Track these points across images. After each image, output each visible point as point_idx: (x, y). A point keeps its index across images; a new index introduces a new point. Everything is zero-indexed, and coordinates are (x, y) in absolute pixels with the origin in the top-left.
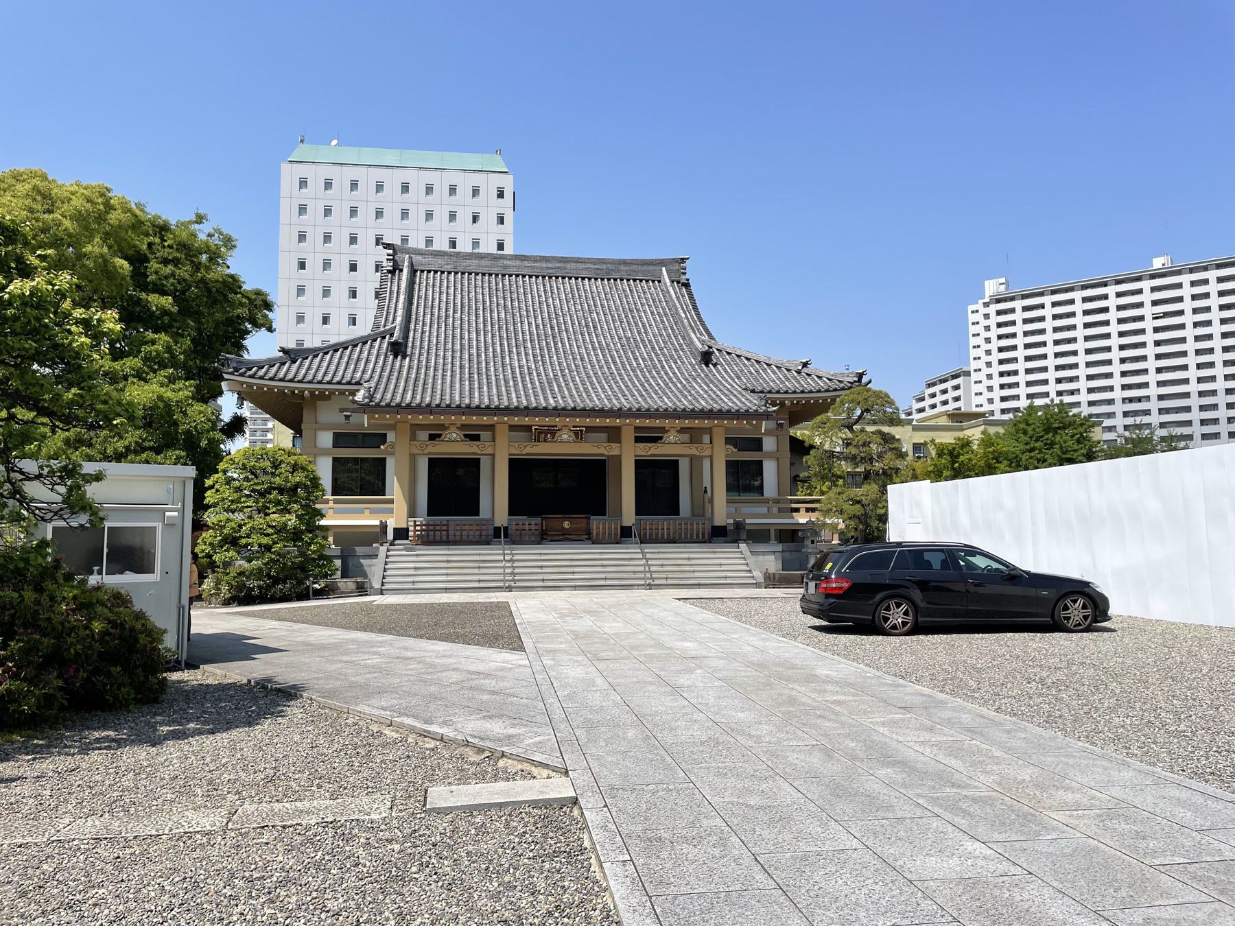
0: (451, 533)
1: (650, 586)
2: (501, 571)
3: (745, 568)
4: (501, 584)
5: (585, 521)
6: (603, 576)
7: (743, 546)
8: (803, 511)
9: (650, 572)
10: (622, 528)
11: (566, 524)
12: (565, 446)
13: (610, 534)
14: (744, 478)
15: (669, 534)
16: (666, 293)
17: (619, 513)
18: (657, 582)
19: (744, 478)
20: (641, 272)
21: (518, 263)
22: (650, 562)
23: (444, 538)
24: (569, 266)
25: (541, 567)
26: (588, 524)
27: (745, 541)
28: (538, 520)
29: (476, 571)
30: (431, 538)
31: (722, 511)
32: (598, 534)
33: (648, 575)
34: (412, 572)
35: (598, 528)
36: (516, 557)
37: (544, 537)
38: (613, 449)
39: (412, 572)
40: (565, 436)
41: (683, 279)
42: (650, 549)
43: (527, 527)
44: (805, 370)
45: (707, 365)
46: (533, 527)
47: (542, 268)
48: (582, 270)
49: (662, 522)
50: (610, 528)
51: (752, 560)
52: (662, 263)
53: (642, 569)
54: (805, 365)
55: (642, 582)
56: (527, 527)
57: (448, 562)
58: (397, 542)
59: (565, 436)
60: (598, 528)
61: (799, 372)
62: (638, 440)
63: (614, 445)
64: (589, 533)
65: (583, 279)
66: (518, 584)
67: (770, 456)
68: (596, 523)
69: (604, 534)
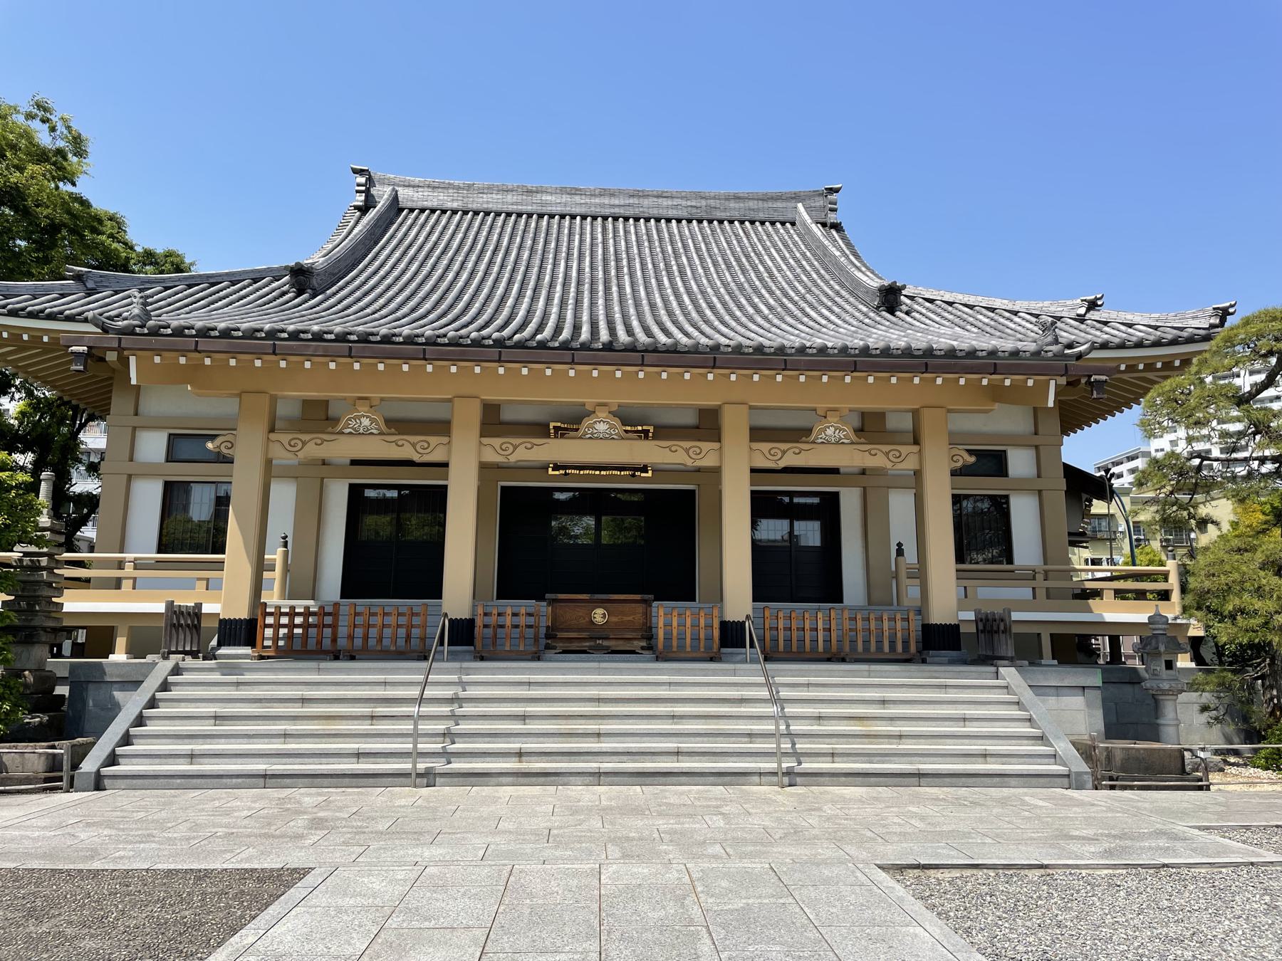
0: (343, 631)
1: (791, 778)
2: (407, 727)
3: (1026, 730)
4: (406, 766)
5: (640, 608)
6: (671, 745)
7: (1009, 673)
8: (1108, 596)
9: (786, 718)
10: (724, 625)
11: (599, 615)
12: (601, 449)
13: (696, 639)
14: (983, 533)
15: (828, 641)
16: (806, 235)
17: (718, 596)
18: (808, 765)
19: (983, 533)
20: (768, 214)
21: (565, 198)
22: (790, 710)
23: (327, 643)
24: (646, 202)
25: (524, 718)
26: (647, 615)
27: (1012, 661)
28: (543, 608)
29: (365, 727)
30: (312, 644)
31: (947, 597)
32: (668, 638)
33: (786, 746)
34: (208, 727)
35: (668, 624)
36: (472, 692)
37: (555, 643)
38: (700, 454)
39: (208, 727)
40: (602, 427)
41: (832, 218)
42: (790, 676)
43: (508, 620)
44: (1094, 315)
45: (892, 313)
46: (522, 620)
47: (602, 206)
48: (666, 207)
49: (810, 617)
50: (695, 625)
51: (1042, 707)
52: (796, 197)
53: (769, 727)
54: (1092, 305)
55: (771, 765)
56: (508, 620)
57: (304, 701)
58: (224, 651)
59: (602, 427)
60: (668, 624)
61: (1081, 319)
62: (758, 434)
63: (706, 446)
64: (648, 634)
65: (668, 220)
66: (457, 765)
67: (1023, 486)
68: (667, 616)
69: (682, 638)
